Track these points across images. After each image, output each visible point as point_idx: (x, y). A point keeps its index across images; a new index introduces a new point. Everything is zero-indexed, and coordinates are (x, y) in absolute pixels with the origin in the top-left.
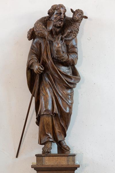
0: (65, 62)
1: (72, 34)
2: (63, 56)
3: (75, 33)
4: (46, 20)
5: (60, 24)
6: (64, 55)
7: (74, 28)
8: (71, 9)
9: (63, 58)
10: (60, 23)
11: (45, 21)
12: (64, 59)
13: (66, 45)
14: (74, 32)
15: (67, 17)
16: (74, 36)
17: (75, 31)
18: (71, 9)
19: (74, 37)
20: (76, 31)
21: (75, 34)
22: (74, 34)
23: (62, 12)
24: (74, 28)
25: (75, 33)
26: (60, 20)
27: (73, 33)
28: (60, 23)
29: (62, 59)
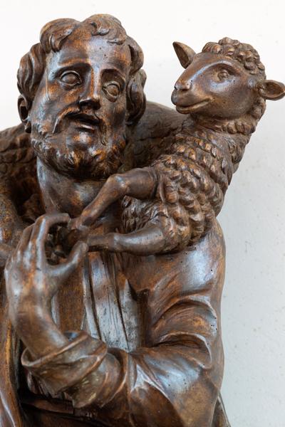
0: (93, 407)
1: (165, 211)
2: (72, 366)
3: (184, 203)
4: (18, 140)
5: (80, 148)
6: (74, 357)
7: (176, 166)
8: (177, 46)
9: (70, 377)
10: (84, 138)
11: (13, 146)
12: (79, 382)
13: (133, 294)
14: (174, 196)
15: (153, 105)
16: (178, 221)
17: (186, 185)
18: (177, 46)
19: (185, 229)
20: (193, 190)
21: (192, 211)
22: (179, 210)
23: (90, 61)
24: (176, 166)
25: (184, 203)
26: (82, 115)
27: (169, 203)
28: (84, 138)
29: (73, 389)
